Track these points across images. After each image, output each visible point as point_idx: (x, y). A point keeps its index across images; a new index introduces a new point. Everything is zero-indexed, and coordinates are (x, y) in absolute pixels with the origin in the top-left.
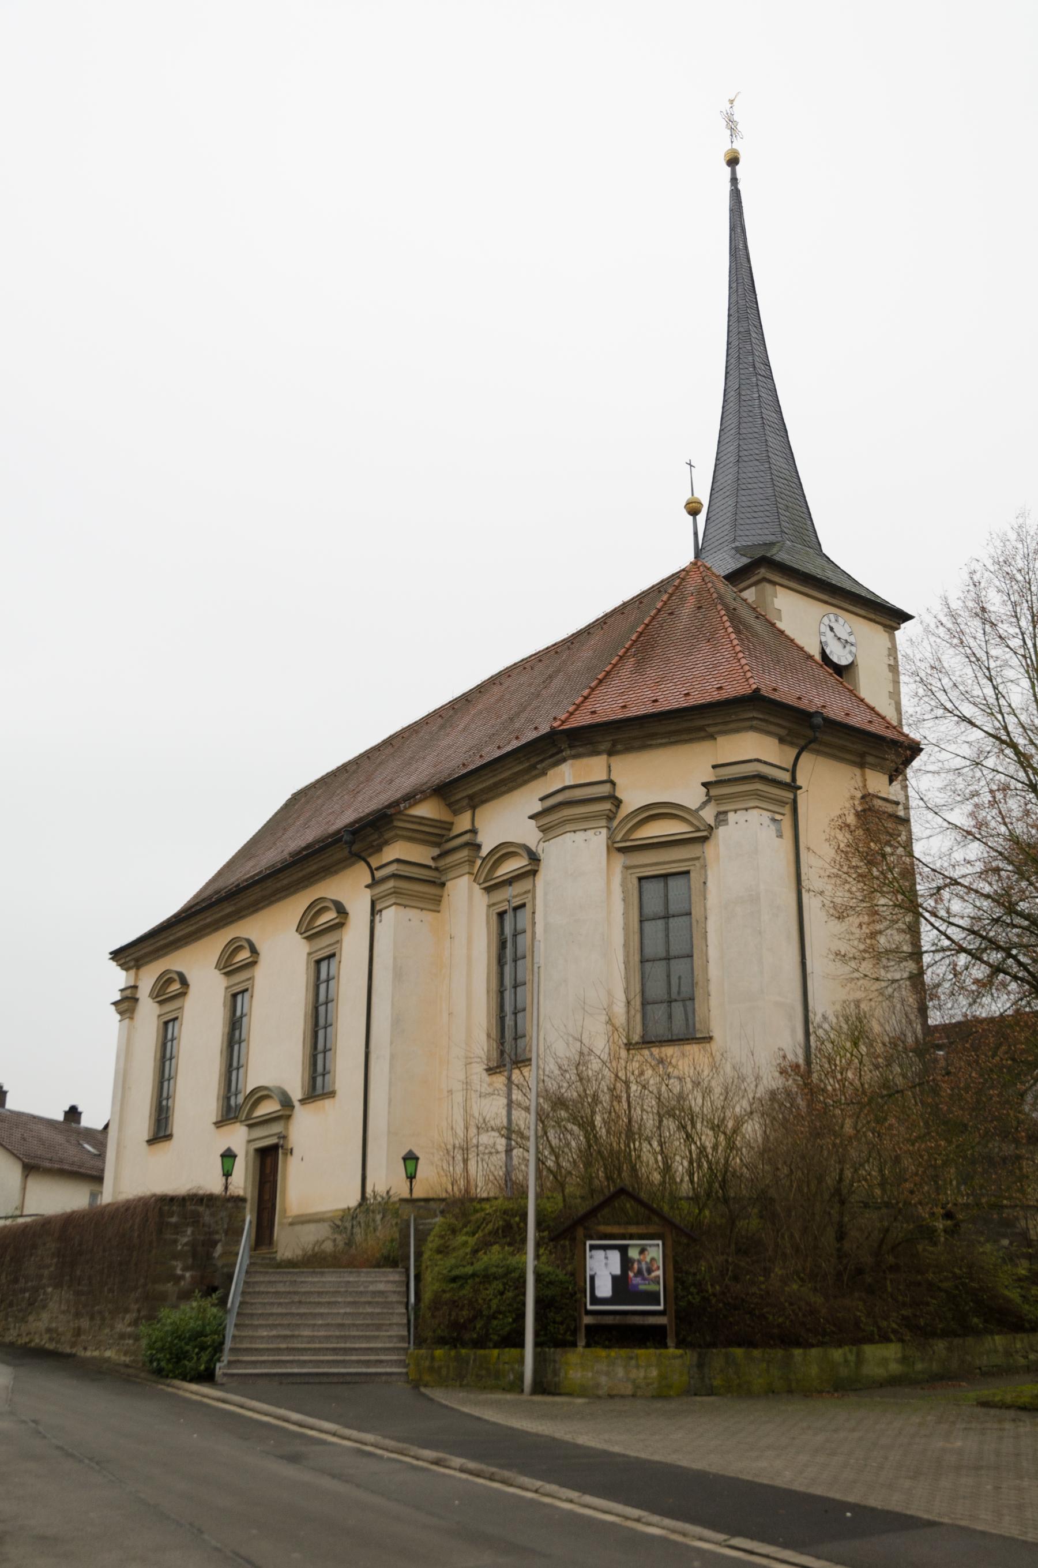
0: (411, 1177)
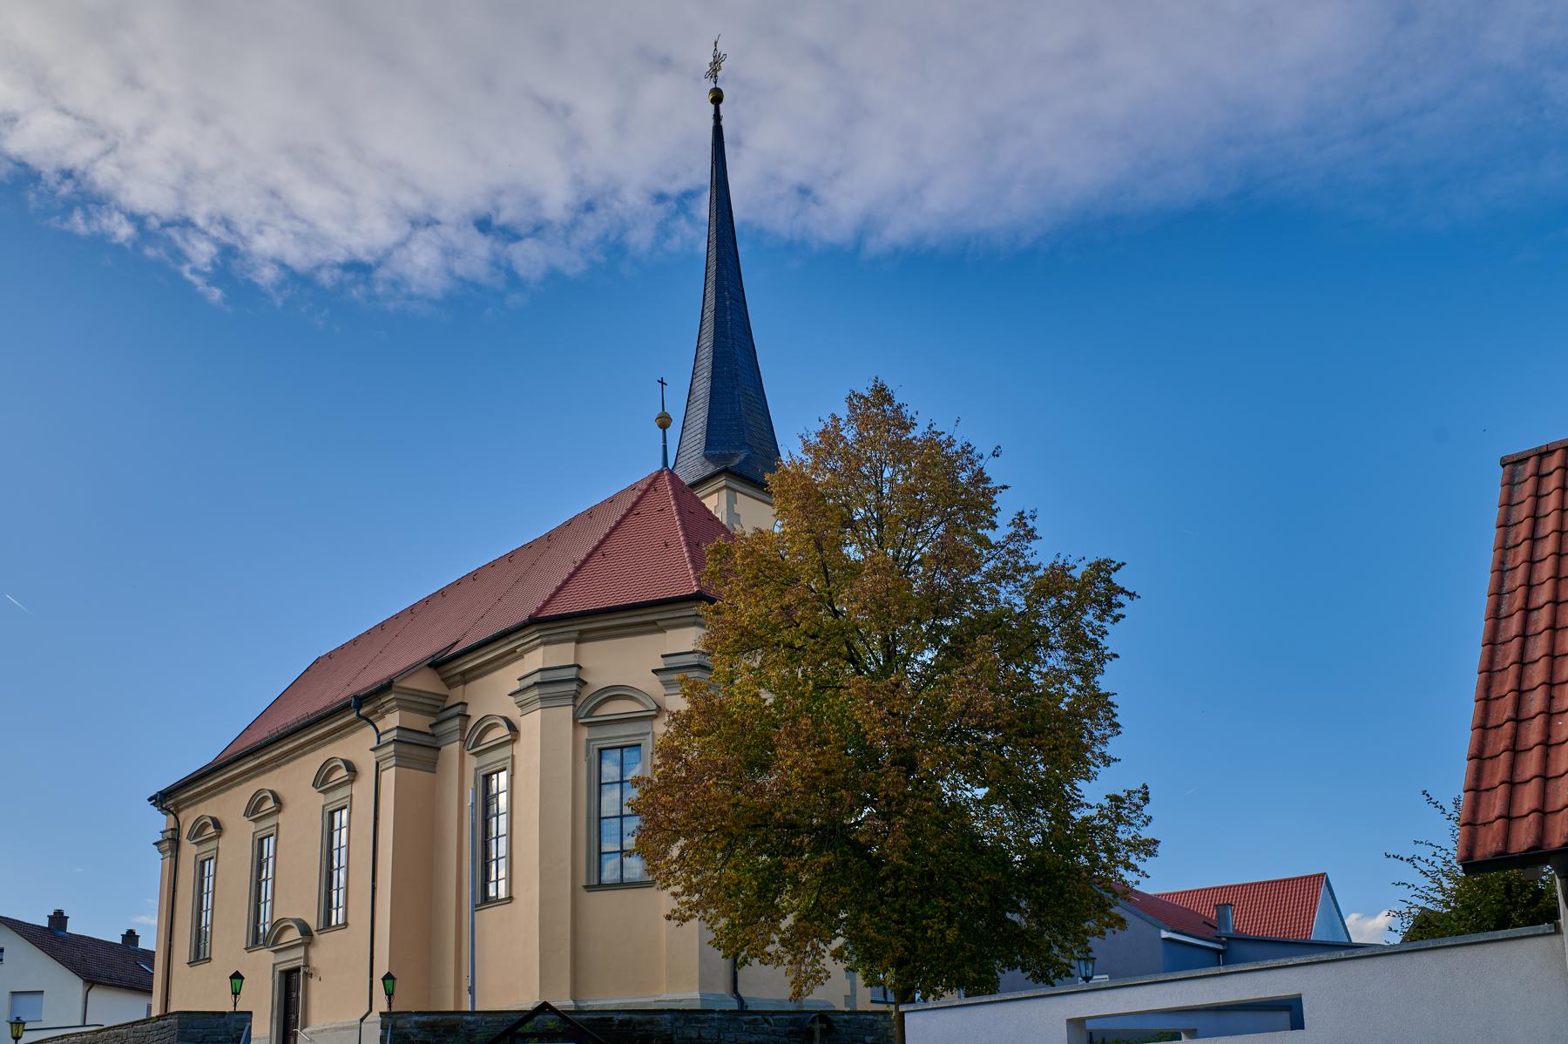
0: (236, 994)
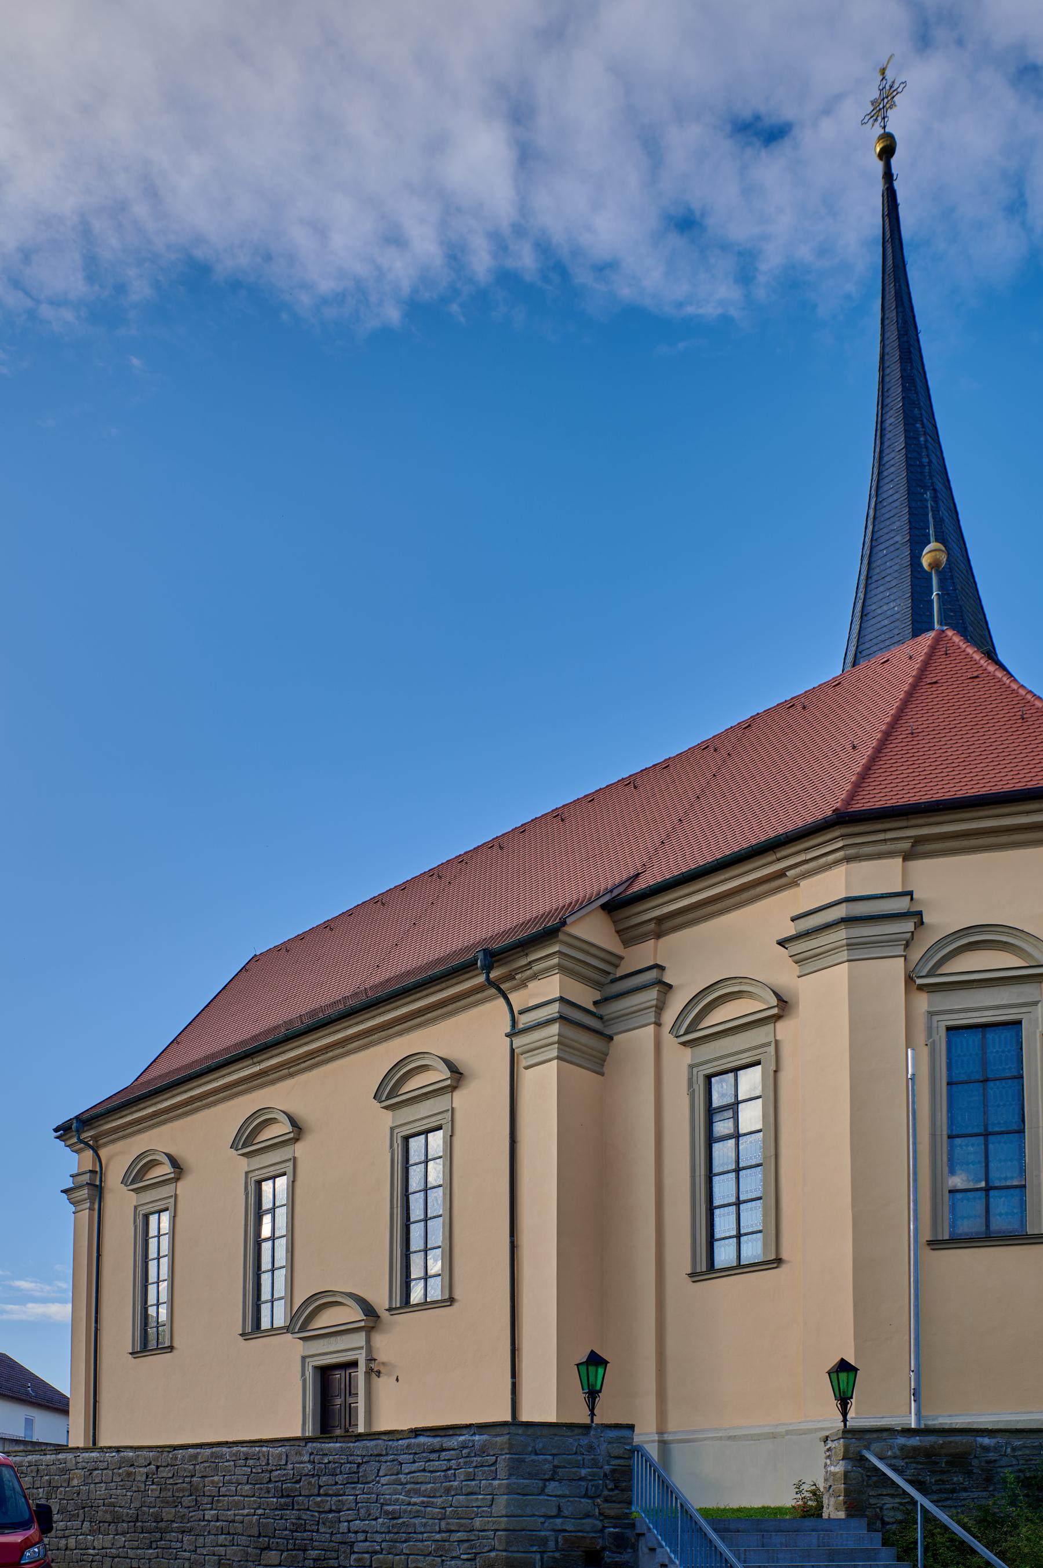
0: (593, 1395)
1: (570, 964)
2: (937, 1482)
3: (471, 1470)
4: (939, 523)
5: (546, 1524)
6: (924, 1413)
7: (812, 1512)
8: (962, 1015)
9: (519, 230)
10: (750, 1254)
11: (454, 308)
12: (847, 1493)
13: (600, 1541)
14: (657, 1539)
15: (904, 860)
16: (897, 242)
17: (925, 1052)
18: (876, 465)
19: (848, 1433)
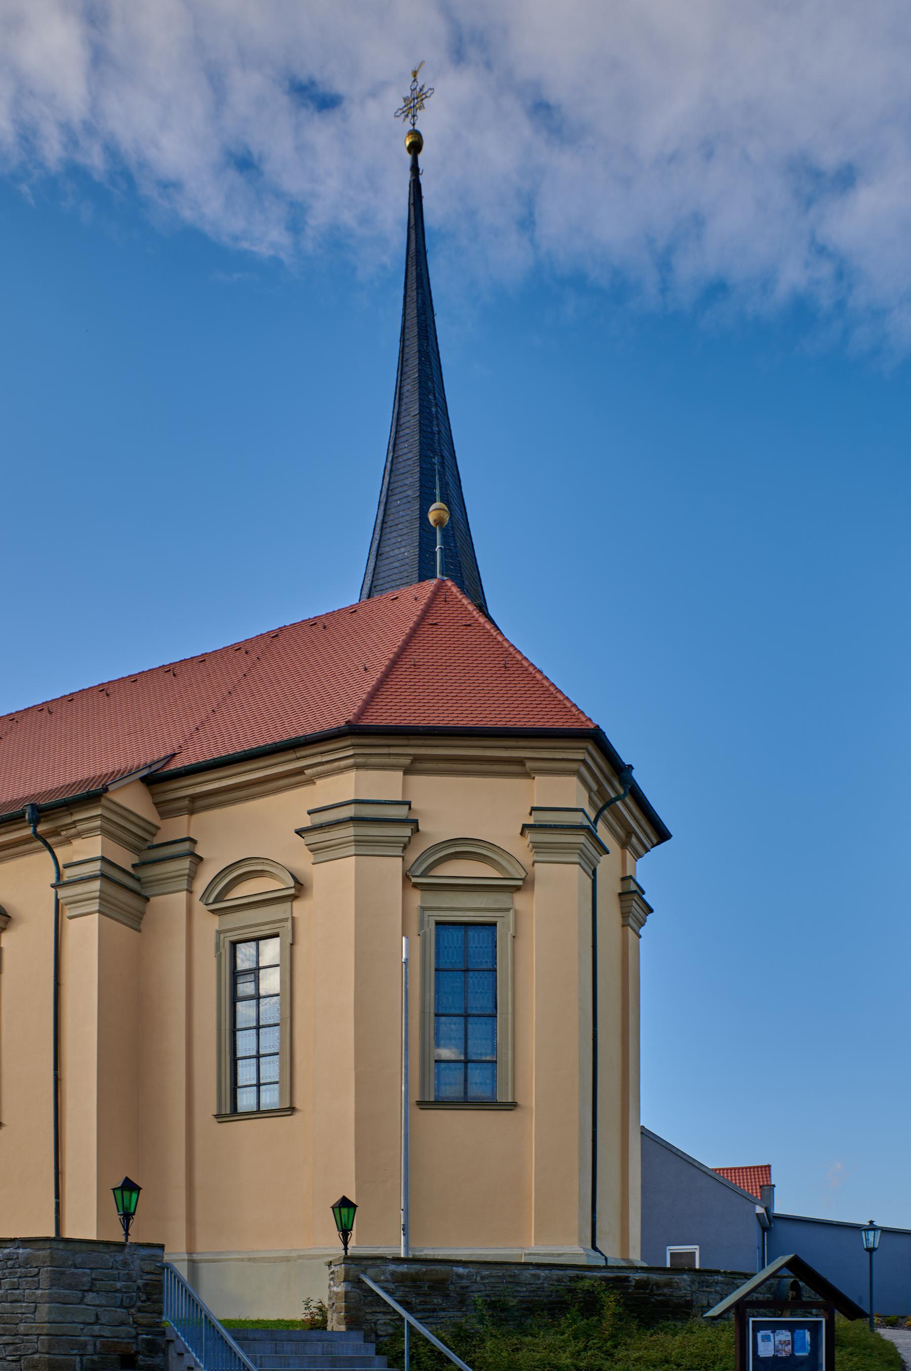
0: (127, 1217)
1: (112, 829)
2: (421, 1303)
3: (15, 1280)
4: (444, 486)
5: (85, 1331)
6: (411, 1245)
7: (319, 1325)
8: (449, 913)
9: (90, 129)
10: (268, 1102)
11: (25, 188)
12: (347, 1309)
13: (134, 1346)
14: (184, 1345)
15: (405, 773)
16: (420, 231)
17: (417, 941)
18: (394, 424)
19: (348, 1259)
